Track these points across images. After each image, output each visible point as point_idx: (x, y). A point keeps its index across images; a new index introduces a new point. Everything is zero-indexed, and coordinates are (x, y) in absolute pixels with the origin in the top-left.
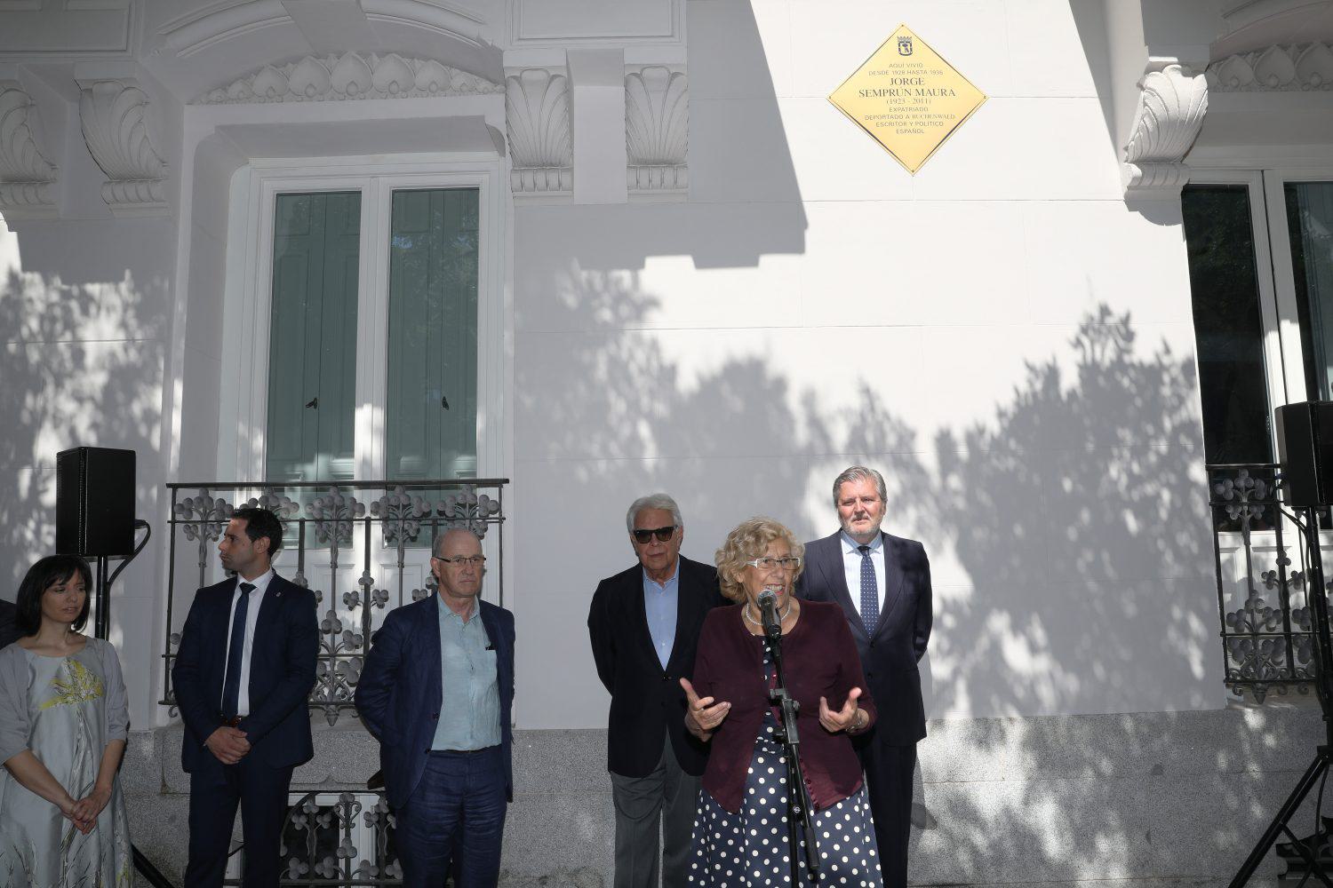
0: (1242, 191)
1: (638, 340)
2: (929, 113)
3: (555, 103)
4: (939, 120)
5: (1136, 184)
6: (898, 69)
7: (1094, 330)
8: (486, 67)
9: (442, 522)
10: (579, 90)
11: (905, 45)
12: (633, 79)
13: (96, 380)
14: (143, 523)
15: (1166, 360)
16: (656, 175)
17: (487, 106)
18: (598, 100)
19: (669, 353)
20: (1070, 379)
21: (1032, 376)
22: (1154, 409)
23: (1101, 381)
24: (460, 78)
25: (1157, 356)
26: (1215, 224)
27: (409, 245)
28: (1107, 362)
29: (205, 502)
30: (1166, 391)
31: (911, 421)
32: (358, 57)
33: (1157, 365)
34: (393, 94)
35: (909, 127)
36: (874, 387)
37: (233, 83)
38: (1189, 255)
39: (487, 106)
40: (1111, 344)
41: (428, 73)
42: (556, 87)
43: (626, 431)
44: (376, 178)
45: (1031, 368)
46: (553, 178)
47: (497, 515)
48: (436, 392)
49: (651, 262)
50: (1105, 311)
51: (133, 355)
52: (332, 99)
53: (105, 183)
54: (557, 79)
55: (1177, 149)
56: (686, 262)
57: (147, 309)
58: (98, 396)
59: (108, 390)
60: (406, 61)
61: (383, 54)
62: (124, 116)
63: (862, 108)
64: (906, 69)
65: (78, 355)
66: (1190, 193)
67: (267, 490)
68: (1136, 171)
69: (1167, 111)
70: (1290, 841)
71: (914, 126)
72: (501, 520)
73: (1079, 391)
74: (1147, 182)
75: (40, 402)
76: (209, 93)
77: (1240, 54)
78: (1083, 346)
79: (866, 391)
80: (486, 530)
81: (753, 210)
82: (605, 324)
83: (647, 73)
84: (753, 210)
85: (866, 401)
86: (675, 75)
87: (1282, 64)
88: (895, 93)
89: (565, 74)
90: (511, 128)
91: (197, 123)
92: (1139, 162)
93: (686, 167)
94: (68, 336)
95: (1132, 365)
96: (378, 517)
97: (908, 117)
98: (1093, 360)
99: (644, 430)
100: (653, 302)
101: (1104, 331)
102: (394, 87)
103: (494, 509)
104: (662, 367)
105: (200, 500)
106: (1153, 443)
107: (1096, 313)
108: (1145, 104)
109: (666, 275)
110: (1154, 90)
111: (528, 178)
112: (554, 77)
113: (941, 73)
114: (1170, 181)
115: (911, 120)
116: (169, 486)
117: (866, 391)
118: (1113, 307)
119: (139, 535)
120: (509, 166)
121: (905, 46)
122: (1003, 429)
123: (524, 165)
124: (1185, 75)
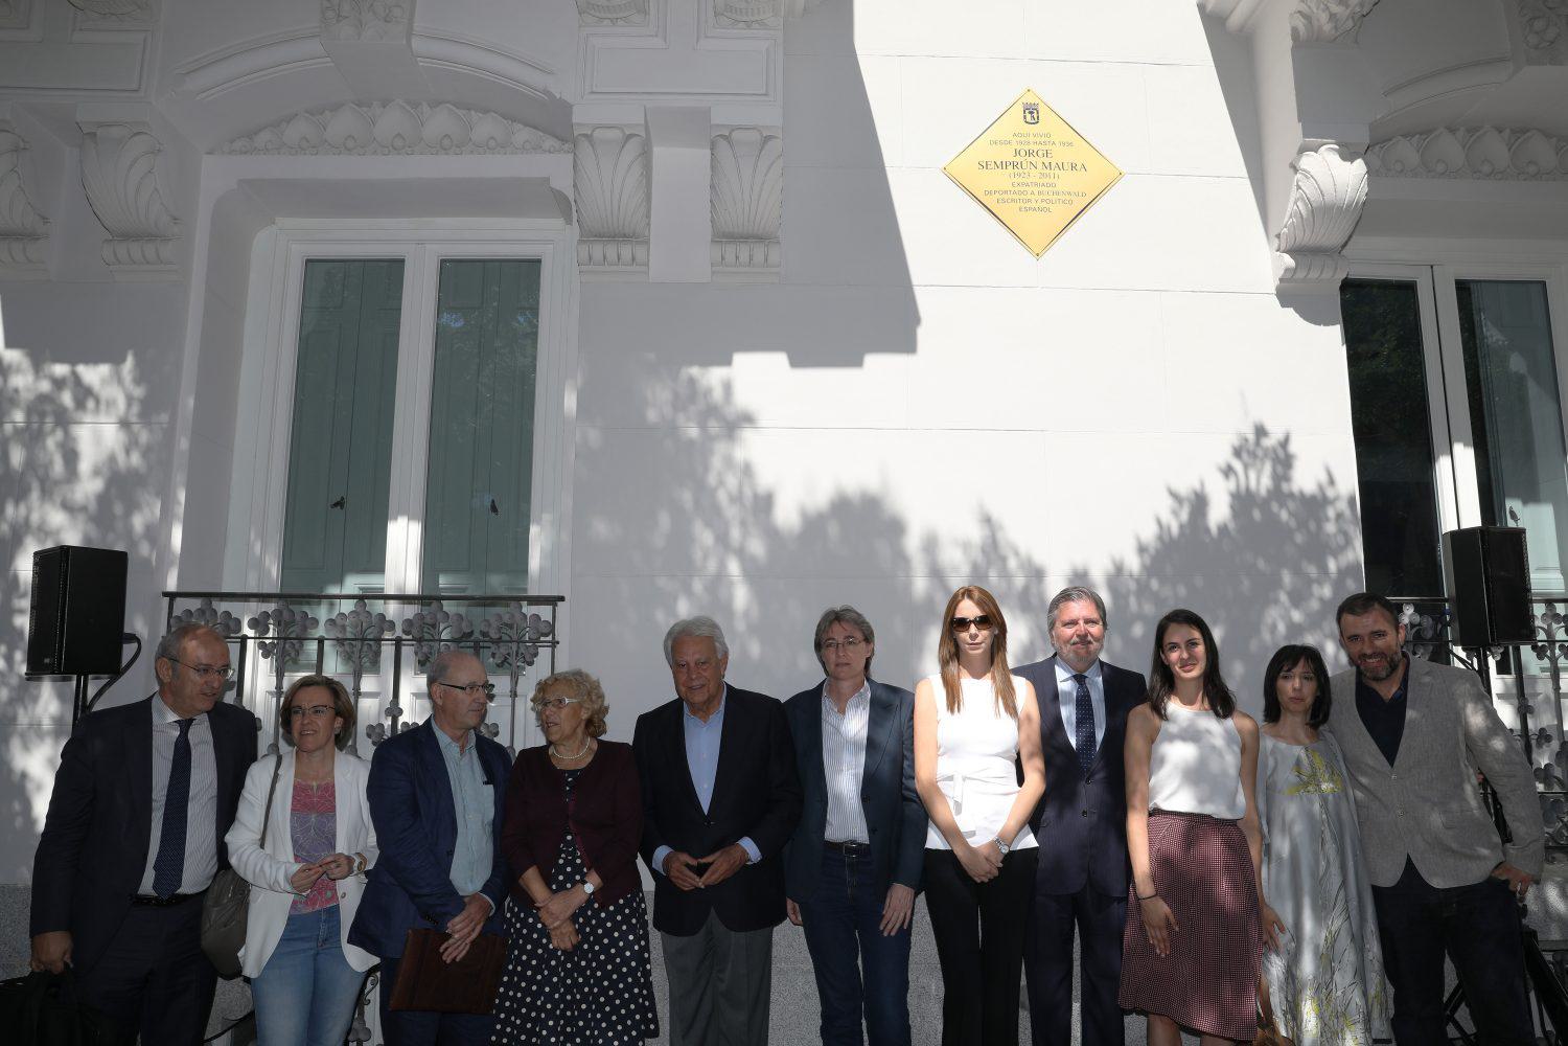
0: (1408, 289)
1: (729, 461)
2: (1059, 188)
3: (630, 167)
4: (1068, 198)
5: (1289, 276)
6: (1023, 139)
7: (1248, 452)
8: (553, 123)
9: (486, 644)
10: (658, 151)
11: (1031, 112)
12: (719, 140)
13: (88, 487)
14: (133, 638)
15: (1330, 493)
16: (744, 252)
17: (554, 168)
18: (679, 164)
19: (765, 479)
20: (1219, 512)
21: (1176, 505)
22: (1319, 549)
23: (1257, 515)
24: (523, 134)
25: (1321, 488)
26: (1378, 326)
27: (460, 324)
28: (1263, 492)
29: (208, 614)
30: (1330, 528)
31: (1040, 558)
32: (408, 107)
33: (1319, 497)
34: (446, 150)
35: (1034, 205)
36: (996, 515)
37: (260, 130)
38: (1348, 358)
39: (554, 168)
40: (1268, 468)
41: (486, 127)
42: (632, 148)
43: (712, 566)
44: (422, 246)
45: (1174, 495)
46: (626, 251)
47: (550, 638)
48: (482, 503)
49: (739, 359)
50: (1261, 432)
51: (136, 459)
52: (375, 153)
53: (106, 240)
54: (632, 140)
55: (1336, 239)
56: (780, 359)
57: (152, 404)
58: (93, 506)
59: (103, 499)
60: (461, 112)
61: (435, 104)
62: (131, 166)
63: (984, 182)
64: (1031, 139)
65: (71, 456)
66: (1347, 286)
67: (281, 603)
68: (1289, 261)
69: (1323, 196)
70: (1459, 1036)
71: (1029, 189)
72: (554, 644)
73: (1231, 526)
74: (1301, 275)
75: (22, 510)
76: (232, 142)
77: (1405, 136)
78: (1236, 474)
79: (987, 520)
80: (536, 655)
81: (856, 301)
82: (691, 442)
83: (736, 135)
84: (856, 301)
85: (987, 532)
86: (768, 139)
87: (1450, 148)
88: (1019, 166)
89: (643, 134)
90: (579, 194)
91: (217, 176)
92: (1291, 252)
93: (778, 242)
94: (59, 434)
95: (1291, 495)
96: (410, 637)
97: (1033, 193)
98: (1248, 489)
99: (734, 567)
100: (747, 419)
101: (1260, 453)
102: (446, 142)
103: (545, 631)
104: (756, 496)
105: (202, 612)
106: (1316, 589)
107: (1251, 437)
108: (1299, 187)
109: (757, 378)
110: (1309, 173)
111: (597, 250)
112: (630, 136)
113: (1070, 144)
114: (1327, 275)
115: (1036, 197)
116: (166, 594)
117: (987, 520)
118: (1269, 426)
119: (128, 650)
120: (577, 237)
121: (1031, 113)
122: (1144, 567)
123: (594, 235)
124: (1344, 158)
